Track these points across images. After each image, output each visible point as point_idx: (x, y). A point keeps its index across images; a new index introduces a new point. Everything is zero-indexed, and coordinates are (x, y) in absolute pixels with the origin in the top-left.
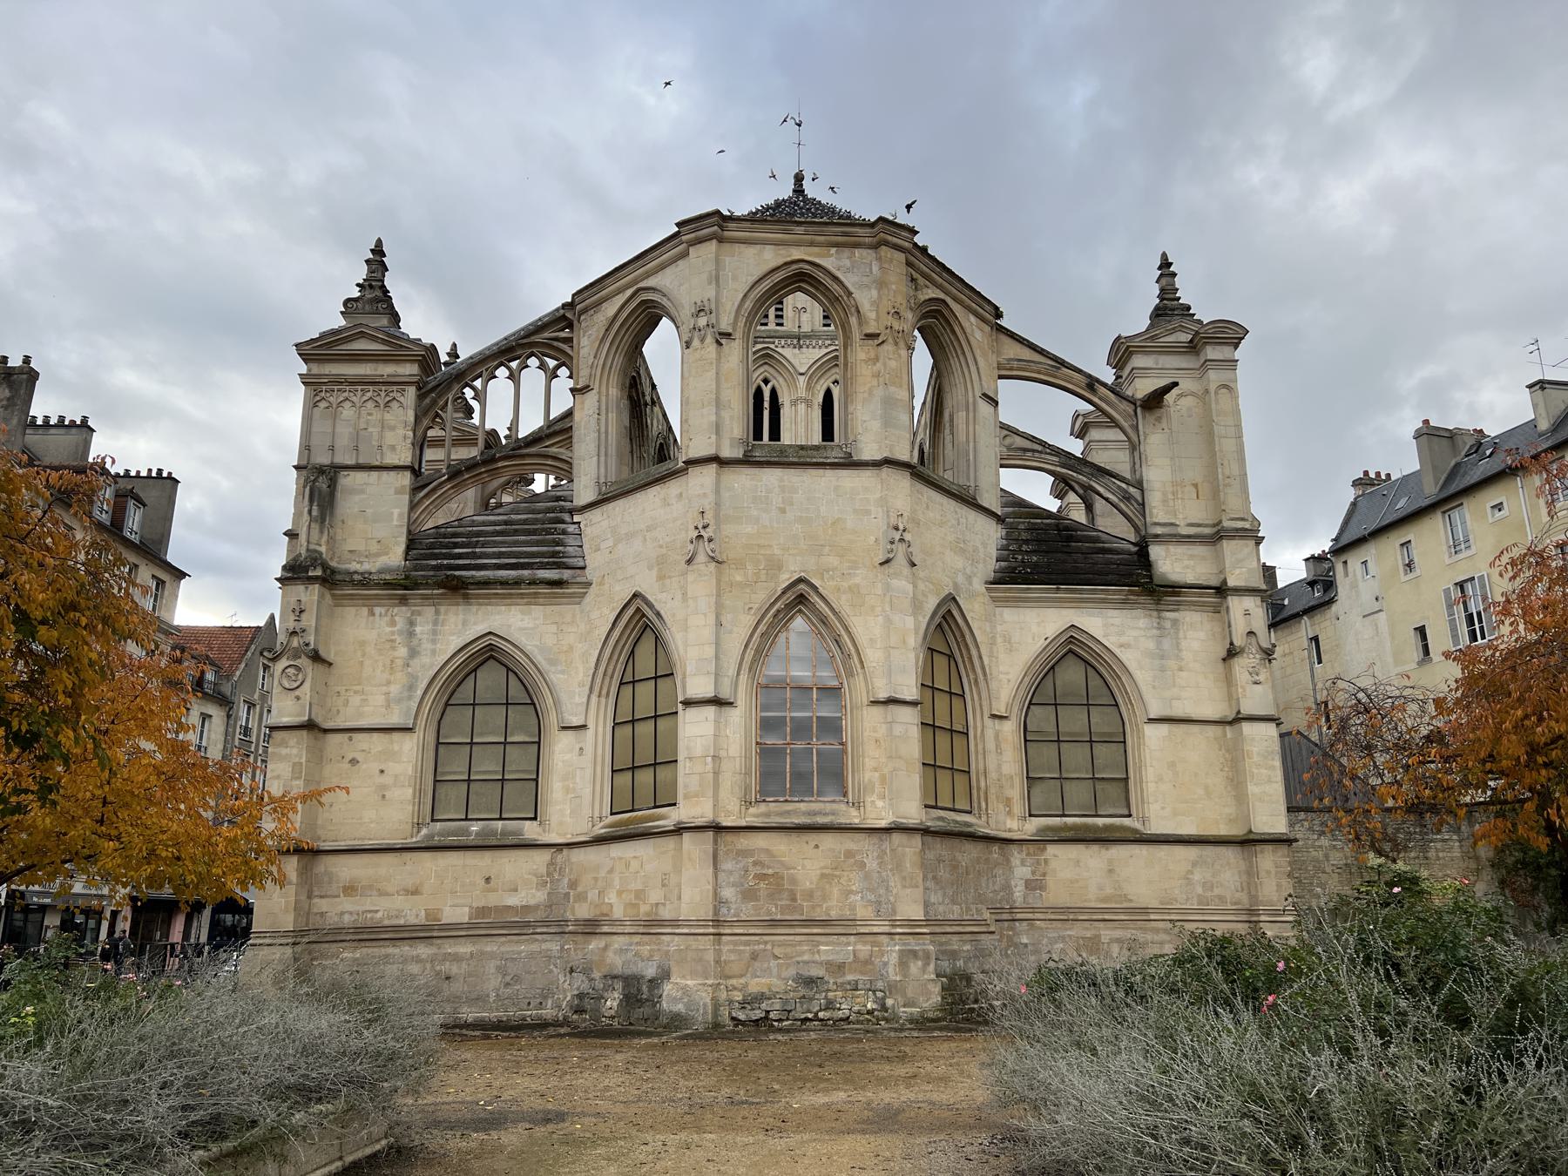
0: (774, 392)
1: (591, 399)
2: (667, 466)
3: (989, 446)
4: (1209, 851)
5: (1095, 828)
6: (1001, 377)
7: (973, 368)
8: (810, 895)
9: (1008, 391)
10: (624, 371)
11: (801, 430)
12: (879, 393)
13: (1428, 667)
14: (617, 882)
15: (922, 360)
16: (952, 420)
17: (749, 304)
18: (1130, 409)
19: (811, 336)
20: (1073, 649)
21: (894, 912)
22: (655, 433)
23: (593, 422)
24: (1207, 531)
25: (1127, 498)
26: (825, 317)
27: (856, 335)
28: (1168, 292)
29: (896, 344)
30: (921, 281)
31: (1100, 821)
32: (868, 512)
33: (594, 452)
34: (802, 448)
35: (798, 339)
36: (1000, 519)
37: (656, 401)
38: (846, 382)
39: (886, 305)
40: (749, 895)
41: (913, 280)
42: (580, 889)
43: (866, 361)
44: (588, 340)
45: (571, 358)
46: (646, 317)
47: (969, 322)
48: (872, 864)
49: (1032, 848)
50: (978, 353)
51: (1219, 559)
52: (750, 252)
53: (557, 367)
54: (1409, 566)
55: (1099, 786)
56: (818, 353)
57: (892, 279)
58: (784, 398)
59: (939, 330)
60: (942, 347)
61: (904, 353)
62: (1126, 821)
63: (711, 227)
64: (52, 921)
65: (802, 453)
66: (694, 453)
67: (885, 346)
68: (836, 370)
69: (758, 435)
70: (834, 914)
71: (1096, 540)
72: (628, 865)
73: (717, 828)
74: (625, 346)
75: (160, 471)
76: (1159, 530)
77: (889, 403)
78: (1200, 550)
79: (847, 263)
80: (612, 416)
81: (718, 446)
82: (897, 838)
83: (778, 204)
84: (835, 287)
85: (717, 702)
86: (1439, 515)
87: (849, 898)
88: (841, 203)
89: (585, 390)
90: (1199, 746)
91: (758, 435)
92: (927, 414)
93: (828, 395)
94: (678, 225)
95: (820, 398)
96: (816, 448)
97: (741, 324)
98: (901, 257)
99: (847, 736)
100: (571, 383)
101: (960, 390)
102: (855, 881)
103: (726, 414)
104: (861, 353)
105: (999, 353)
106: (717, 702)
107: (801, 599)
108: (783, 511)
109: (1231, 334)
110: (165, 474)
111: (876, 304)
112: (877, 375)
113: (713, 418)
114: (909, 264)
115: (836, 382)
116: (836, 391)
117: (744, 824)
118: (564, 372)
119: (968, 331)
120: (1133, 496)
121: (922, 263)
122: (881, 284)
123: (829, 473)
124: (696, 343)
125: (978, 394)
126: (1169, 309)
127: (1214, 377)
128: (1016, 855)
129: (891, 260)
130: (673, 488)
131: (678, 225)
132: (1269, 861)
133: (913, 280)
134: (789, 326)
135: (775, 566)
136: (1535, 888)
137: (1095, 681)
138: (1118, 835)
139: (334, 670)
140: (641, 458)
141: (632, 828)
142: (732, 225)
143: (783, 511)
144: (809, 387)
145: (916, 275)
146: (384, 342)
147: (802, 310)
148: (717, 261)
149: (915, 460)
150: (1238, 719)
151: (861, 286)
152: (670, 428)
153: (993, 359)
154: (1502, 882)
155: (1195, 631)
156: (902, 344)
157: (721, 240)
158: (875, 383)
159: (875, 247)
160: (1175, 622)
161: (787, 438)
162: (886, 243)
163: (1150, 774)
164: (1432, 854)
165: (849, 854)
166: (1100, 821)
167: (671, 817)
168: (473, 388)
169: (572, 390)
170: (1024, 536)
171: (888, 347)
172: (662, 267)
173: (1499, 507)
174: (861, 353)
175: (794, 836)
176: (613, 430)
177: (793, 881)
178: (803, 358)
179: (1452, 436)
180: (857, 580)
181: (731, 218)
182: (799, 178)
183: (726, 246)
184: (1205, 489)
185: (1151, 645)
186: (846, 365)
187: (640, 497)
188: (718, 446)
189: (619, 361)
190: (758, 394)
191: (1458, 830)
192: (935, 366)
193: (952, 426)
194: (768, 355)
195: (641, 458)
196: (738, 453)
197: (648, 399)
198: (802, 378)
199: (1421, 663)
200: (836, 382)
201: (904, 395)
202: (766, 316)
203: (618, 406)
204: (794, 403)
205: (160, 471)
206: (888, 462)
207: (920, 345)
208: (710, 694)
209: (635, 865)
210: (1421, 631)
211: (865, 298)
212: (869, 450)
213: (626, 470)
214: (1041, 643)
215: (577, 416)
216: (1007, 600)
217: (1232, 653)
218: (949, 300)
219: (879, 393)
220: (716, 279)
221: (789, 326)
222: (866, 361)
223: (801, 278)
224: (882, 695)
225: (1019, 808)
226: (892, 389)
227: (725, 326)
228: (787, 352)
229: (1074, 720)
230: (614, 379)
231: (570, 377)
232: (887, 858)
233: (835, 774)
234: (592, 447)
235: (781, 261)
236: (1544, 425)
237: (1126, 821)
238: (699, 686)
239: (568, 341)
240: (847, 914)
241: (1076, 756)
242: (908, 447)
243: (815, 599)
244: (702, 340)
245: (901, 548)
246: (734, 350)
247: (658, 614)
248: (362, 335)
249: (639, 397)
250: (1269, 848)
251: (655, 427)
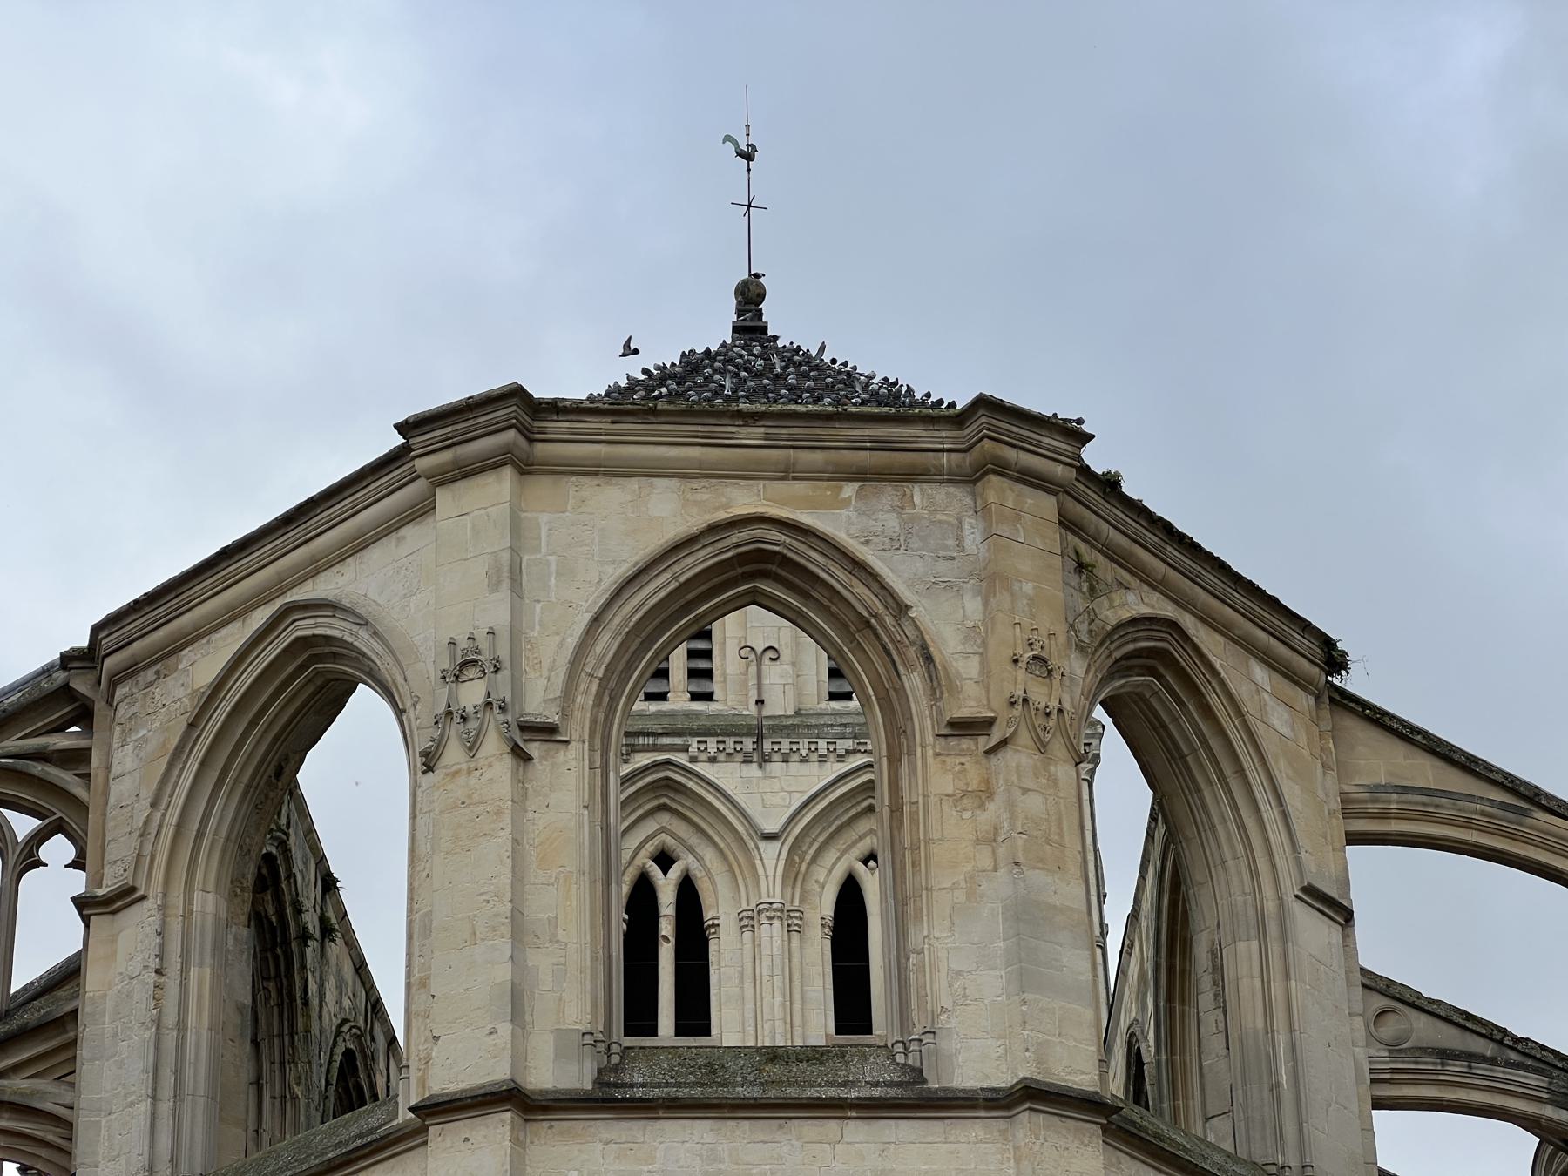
0: (688, 893)
1: (135, 930)
2: (366, 1121)
3: (1335, 1048)
6: (1355, 839)
7: (1270, 813)
9: (1375, 875)
10: (239, 845)
11: (774, 1003)
12: (1000, 886)
15: (1122, 793)
16: (1217, 968)
17: (606, 644)
19: (797, 726)
22: (330, 1021)
23: (141, 1005)
26: (834, 673)
27: (924, 725)
29: (1042, 747)
30: (1106, 570)
33: (144, 1089)
34: (773, 1055)
35: (759, 738)
37: (335, 927)
38: (897, 857)
39: (1009, 640)
41: (1081, 567)
43: (957, 799)
44: (136, 757)
45: (82, 807)
46: (310, 684)
47: (1252, 684)
50: (1281, 769)
52: (609, 497)
53: (40, 837)
56: (816, 776)
57: (1026, 566)
58: (720, 907)
59: (1164, 705)
60: (1175, 755)
61: (1064, 771)
63: (493, 434)
64: (142, 754)
65: (773, 1070)
66: (447, 1079)
67: (1009, 757)
68: (865, 825)
69: (640, 1017)
74: (255, 746)
77: (1027, 916)
79: (892, 523)
80: (201, 976)
81: (519, 1057)
83: (692, 364)
84: (859, 593)
88: (874, 354)
89: (125, 897)
91: (640, 1017)
92: (1144, 954)
93: (850, 898)
94: (402, 428)
95: (826, 904)
96: (814, 1055)
97: (585, 699)
98: (1046, 505)
100: (78, 882)
101: (1237, 872)
103: (542, 961)
104: (939, 775)
105: (1343, 771)
111: (978, 636)
112: (991, 839)
113: (504, 973)
114: (1068, 523)
115: (870, 858)
116: (872, 886)
118: (58, 849)
119: (1249, 707)
121: (1104, 520)
122: (991, 581)
123: (858, 1134)
124: (453, 754)
125: (1291, 887)
129: (1018, 513)
131: (402, 428)
133: (1081, 567)
134: (731, 698)
139: (530, 766)
140: (286, 1098)
144: (792, 874)
145: (1088, 554)
147: (766, 657)
148: (516, 527)
149: (1116, 1087)
151: (935, 587)
152: (376, 1007)
153: (1328, 789)
156: (1058, 748)
157: (526, 468)
158: (985, 860)
159: (971, 478)
161: (731, 1024)
162: (1001, 468)
169: (81, 903)
171: (1019, 758)
172: (358, 545)
174: (939, 775)
176: (200, 1019)
178: (773, 792)
181: (555, 408)
182: (750, 295)
183: (541, 486)
186: (896, 809)
188: (519, 1057)
189: (225, 813)
190: (642, 896)
192: (1159, 811)
193: (1219, 983)
194: (669, 785)
195: (286, 1098)
196: (579, 1076)
197: (311, 920)
198: (770, 850)
200: (870, 858)
201: (1070, 893)
202: (663, 674)
203: (218, 947)
204: (749, 921)
206: (1033, 1095)
207: (1113, 747)
211: (947, 621)
212: (973, 1063)
213: (236, 1137)
215: (93, 980)
218: (1188, 622)
219: (1000, 886)
221: (731, 698)
222: (957, 799)
223: (761, 567)
226: (1037, 877)
227: (538, 703)
228: (728, 775)
230: (209, 868)
231: (78, 864)
234: (136, 1071)
235: (695, 522)
239: (77, 759)
242: (1092, 1049)
244: (472, 747)
246: (565, 775)
249: (282, 910)
251: (331, 1002)
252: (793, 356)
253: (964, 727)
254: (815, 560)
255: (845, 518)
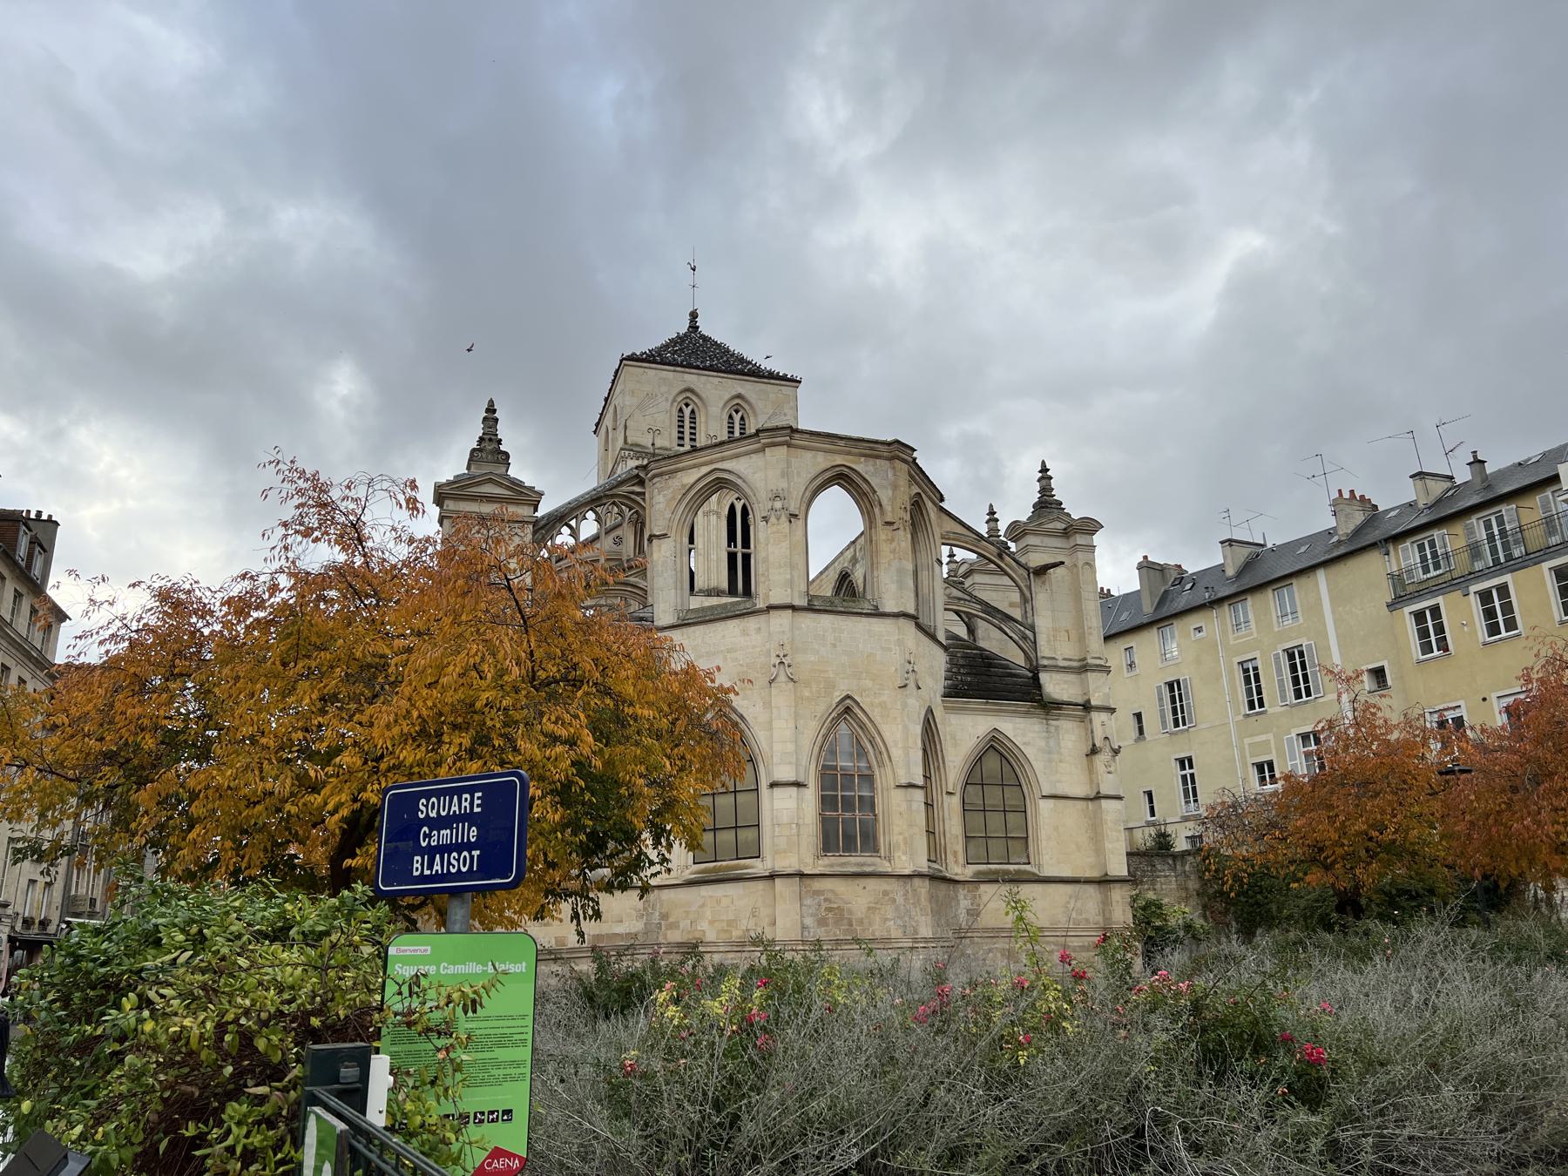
4: (1077, 887)
5: (1007, 872)
8: (861, 922)
13: (1142, 743)
14: (708, 914)
18: (1025, 574)
20: (995, 746)
21: (916, 932)
24: (1075, 664)
25: (1025, 638)
27: (879, 522)
28: (1046, 490)
31: (1011, 867)
32: (890, 650)
36: (945, 648)
40: (822, 922)
42: (671, 920)
48: (900, 900)
49: (971, 886)
51: (1084, 685)
54: (1131, 666)
55: (1010, 843)
62: (1027, 867)
70: (878, 935)
71: (1007, 667)
72: (719, 902)
73: (802, 875)
75: (39, 513)
76: (1045, 662)
78: (1071, 677)
82: (917, 881)
84: (864, 486)
85: (798, 784)
86: (1155, 630)
87: (885, 925)
90: (1072, 814)
99: (879, 810)
102: (889, 911)
106: (798, 784)
107: (848, 710)
108: (834, 646)
109: (1090, 527)
110: (44, 517)
112: (893, 551)
117: (816, 872)
120: (1027, 637)
123: (864, 620)
126: (1047, 504)
127: (1081, 556)
128: (962, 892)
130: (752, 623)
132: (1120, 895)
135: (831, 686)
136: (1227, 911)
137: (1006, 768)
138: (1025, 877)
141: (721, 875)
142: (797, 436)
143: (834, 646)
146: (508, 488)
150: (1098, 797)
154: (1205, 907)
155: (1069, 733)
157: (789, 445)
160: (1057, 727)
162: (899, 458)
163: (1043, 834)
164: (1158, 886)
165: (885, 893)
166: (1011, 867)
167: (758, 867)
168: (570, 527)
170: (961, 662)
171: (901, 532)
172: (737, 456)
173: (1199, 629)
175: (850, 881)
177: (850, 912)
179: (1162, 569)
180: (884, 698)
184: (1073, 634)
185: (1043, 744)
187: (719, 626)
191: (1174, 870)
199: (1137, 741)
205: (39, 513)
208: (792, 779)
209: (725, 902)
210: (1139, 716)
211: (884, 495)
212: (889, 606)
214: (974, 741)
216: (953, 708)
217: (1094, 751)
220: (785, 474)
224: (903, 781)
225: (961, 859)
227: (793, 510)
229: (994, 796)
232: (910, 895)
233: (868, 840)
236: (1230, 572)
237: (1027, 867)
238: (785, 773)
240: (885, 935)
241: (995, 820)
243: (857, 710)
245: (911, 676)
247: (741, 717)
248: (490, 481)
250: (1118, 885)
252: (706, 339)
253: (888, 523)
254: (855, 477)
255: (862, 466)
